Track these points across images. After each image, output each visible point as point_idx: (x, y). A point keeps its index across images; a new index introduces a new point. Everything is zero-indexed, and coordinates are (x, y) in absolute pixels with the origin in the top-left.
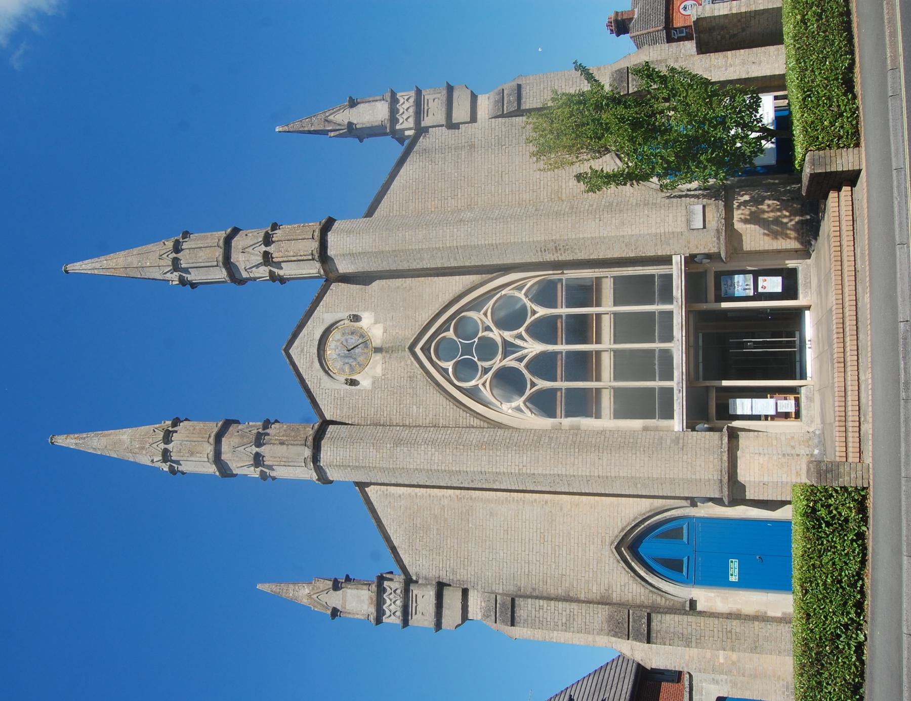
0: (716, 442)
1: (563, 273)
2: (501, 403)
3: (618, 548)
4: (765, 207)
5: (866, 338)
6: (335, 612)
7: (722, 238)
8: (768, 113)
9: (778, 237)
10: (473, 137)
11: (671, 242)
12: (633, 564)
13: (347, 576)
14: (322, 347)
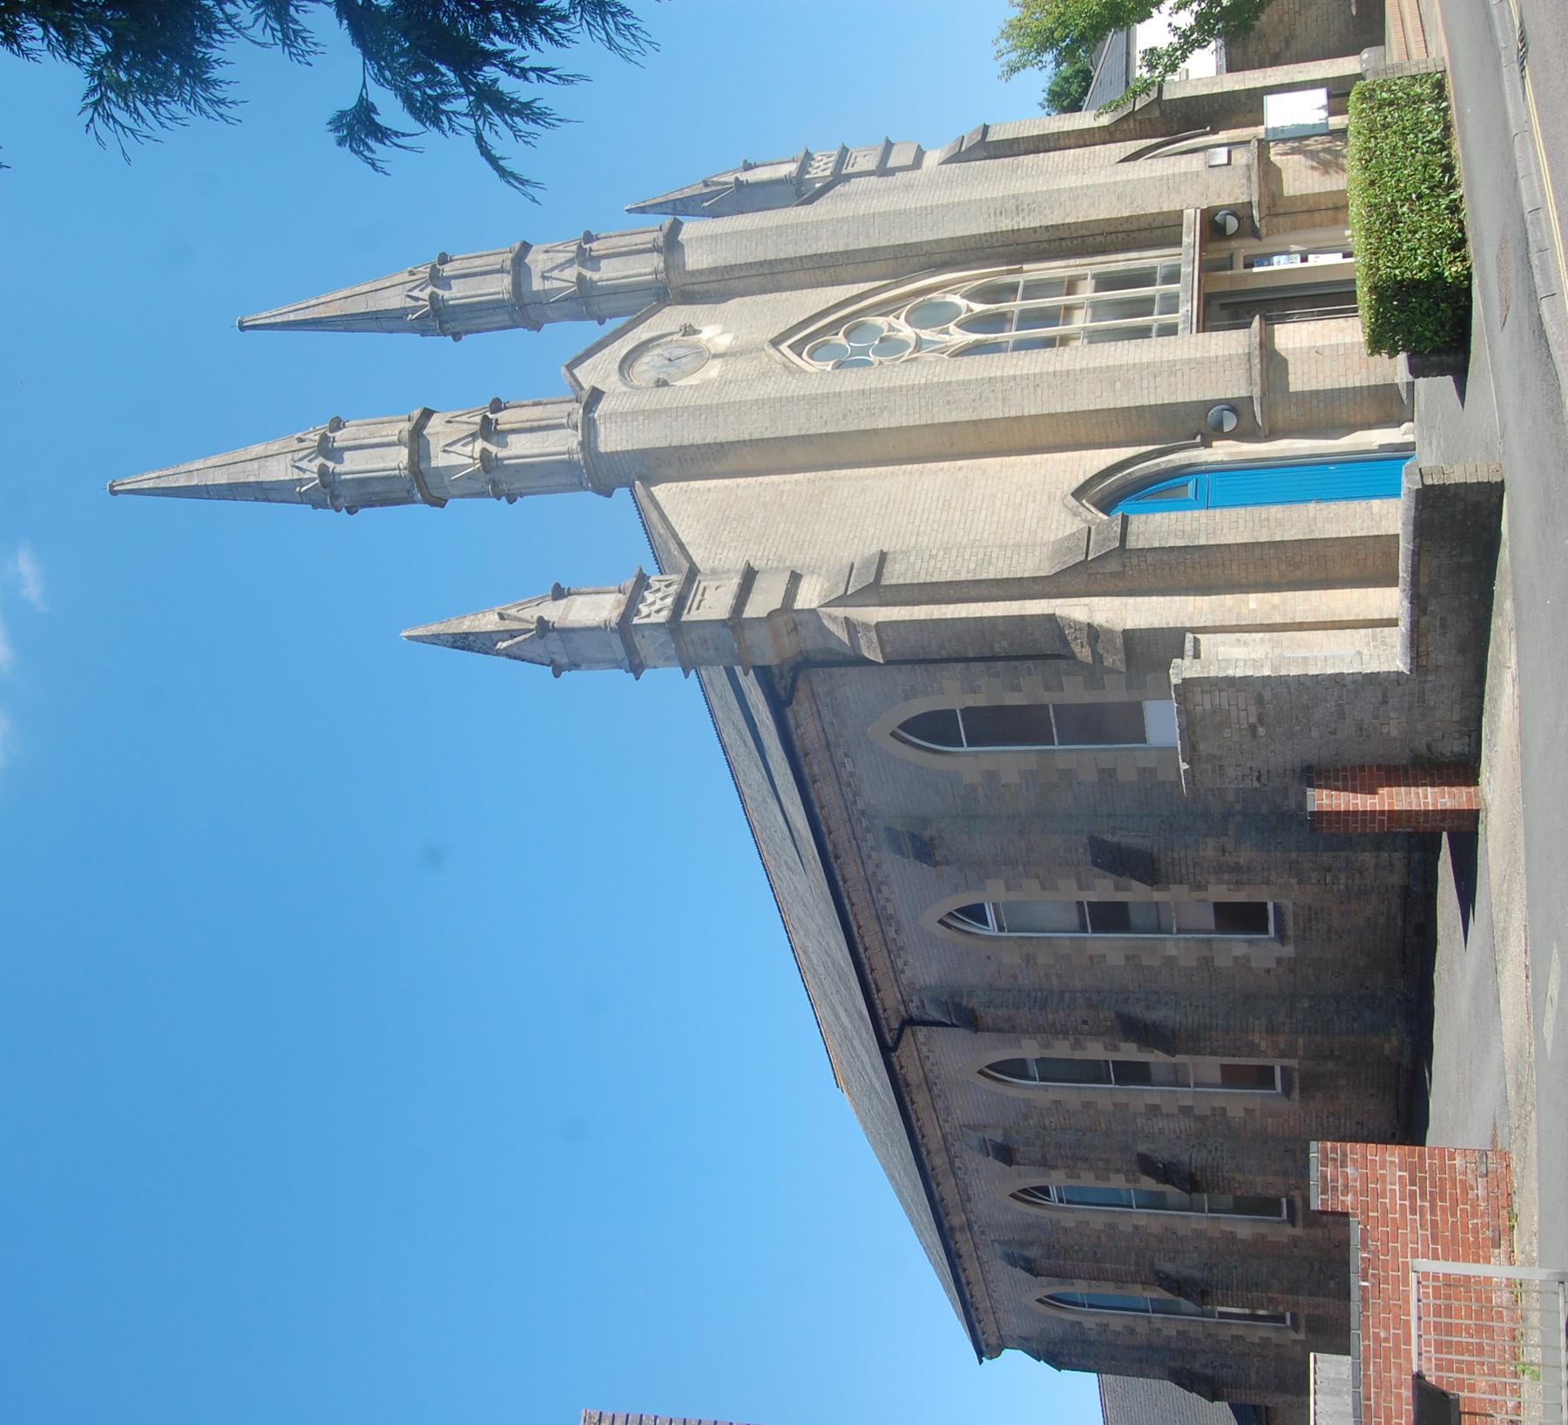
1: (1020, 271)
7: (1255, 178)
9: (1331, 171)
11: (1182, 188)
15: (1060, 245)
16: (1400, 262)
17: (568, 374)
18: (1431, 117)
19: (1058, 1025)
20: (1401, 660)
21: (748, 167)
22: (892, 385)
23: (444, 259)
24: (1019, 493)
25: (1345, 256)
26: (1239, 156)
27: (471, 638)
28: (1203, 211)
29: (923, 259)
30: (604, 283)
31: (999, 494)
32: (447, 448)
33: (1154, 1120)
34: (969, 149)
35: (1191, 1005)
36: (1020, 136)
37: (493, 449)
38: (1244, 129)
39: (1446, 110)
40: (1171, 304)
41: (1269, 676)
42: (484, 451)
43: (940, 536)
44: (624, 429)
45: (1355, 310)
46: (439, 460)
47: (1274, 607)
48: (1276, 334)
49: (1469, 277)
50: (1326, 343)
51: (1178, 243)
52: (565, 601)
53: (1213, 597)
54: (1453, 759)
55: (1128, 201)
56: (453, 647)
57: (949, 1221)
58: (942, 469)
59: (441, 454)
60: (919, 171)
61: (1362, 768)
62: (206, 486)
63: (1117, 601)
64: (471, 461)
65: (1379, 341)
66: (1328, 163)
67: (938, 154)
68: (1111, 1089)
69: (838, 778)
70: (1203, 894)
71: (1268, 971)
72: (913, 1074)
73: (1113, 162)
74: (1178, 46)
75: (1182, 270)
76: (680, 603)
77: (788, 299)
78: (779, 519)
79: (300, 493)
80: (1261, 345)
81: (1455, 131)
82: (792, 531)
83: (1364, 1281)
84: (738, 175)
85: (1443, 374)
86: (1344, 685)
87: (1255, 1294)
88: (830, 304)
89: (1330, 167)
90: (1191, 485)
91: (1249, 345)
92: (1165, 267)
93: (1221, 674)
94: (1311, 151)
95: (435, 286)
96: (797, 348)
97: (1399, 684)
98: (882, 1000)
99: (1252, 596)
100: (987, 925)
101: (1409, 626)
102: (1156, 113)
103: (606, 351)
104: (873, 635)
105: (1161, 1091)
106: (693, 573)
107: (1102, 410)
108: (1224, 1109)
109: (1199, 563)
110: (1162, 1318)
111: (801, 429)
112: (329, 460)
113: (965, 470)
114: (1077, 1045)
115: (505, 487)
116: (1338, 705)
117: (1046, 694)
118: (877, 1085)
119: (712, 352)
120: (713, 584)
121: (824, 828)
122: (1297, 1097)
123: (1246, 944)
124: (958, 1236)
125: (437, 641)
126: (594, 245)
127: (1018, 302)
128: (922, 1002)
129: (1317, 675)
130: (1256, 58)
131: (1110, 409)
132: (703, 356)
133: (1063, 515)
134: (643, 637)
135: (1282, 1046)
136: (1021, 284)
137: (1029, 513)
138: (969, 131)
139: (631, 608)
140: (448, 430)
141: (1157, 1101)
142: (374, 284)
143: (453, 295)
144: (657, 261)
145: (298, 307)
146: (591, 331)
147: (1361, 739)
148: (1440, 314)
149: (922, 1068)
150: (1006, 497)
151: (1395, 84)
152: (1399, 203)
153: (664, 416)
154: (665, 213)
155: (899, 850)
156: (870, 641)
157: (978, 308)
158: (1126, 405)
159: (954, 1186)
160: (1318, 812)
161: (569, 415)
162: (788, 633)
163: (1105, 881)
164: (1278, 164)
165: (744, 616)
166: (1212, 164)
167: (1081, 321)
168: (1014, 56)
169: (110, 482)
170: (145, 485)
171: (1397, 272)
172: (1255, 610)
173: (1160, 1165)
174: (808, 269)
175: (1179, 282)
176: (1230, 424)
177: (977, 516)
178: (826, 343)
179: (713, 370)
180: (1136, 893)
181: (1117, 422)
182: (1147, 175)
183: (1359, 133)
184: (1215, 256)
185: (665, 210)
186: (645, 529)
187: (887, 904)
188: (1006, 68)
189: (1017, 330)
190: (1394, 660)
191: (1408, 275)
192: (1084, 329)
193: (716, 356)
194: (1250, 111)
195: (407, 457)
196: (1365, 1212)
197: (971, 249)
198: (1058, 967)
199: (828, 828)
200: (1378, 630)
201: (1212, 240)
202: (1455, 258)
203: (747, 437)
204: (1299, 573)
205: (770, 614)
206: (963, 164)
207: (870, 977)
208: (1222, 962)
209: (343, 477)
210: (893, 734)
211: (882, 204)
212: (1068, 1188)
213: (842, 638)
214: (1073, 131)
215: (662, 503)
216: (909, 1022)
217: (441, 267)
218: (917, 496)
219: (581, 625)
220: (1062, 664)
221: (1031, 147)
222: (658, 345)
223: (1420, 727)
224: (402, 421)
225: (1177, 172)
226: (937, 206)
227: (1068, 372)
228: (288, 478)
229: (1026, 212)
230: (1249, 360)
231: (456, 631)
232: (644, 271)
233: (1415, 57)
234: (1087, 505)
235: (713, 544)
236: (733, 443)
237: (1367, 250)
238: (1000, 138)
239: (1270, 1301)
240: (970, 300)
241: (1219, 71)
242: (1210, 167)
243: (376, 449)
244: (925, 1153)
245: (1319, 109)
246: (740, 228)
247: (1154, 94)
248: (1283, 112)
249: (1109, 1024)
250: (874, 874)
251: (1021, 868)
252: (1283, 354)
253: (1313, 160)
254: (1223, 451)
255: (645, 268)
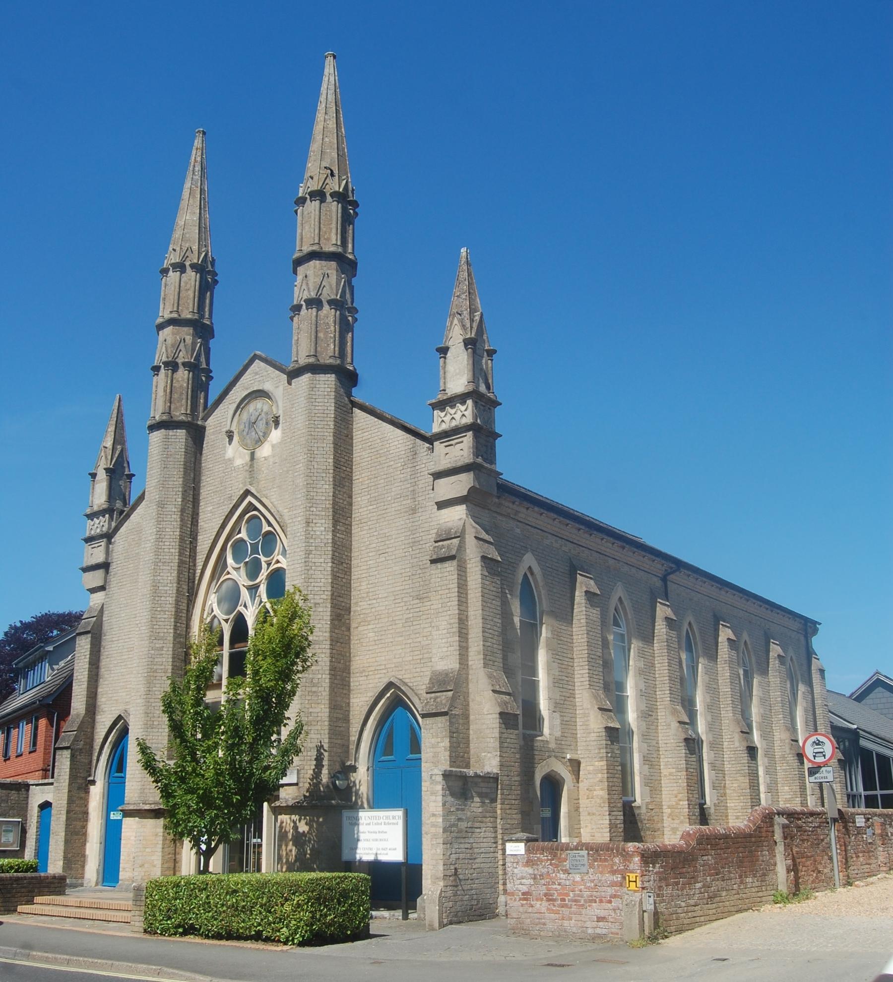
0: (151, 799)
2: (215, 593)
3: (390, 685)
4: (290, 846)
5: (68, 925)
6: (443, 351)
8: (387, 854)
10: (423, 509)
12: (383, 700)
13: (495, 352)
14: (257, 394)
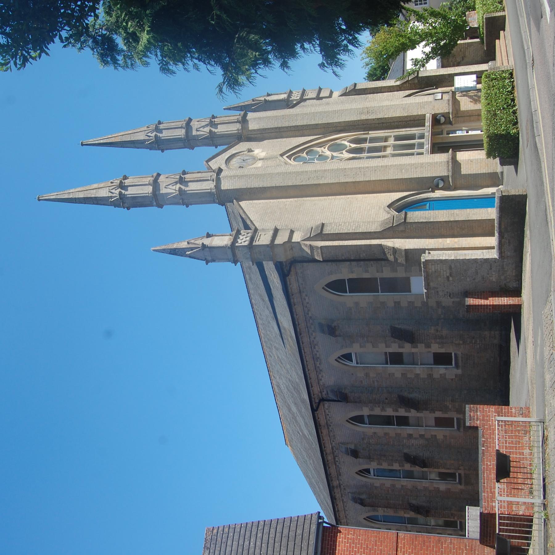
1: (368, 134)
7: (451, 104)
11: (425, 107)
15: (382, 125)
16: (497, 128)
17: (207, 164)
18: (508, 84)
19: (377, 400)
20: (496, 254)
21: (269, 95)
22: (325, 169)
23: (160, 123)
24: (369, 206)
25: (481, 132)
26: (445, 96)
27: (177, 250)
28: (432, 115)
29: (334, 128)
30: (219, 133)
31: (362, 206)
32: (166, 187)
33: (410, 440)
34: (349, 92)
35: (425, 392)
36: (368, 87)
37: (183, 187)
38: (447, 88)
39: (513, 81)
40: (421, 146)
41: (453, 259)
42: (180, 188)
43: (342, 220)
44: (231, 181)
45: (484, 149)
46: (163, 191)
47: (455, 242)
48: (457, 155)
49: (518, 134)
50: (474, 158)
51: (424, 125)
52: (211, 238)
53: (435, 239)
54: (513, 289)
55: (407, 110)
56: (170, 254)
57: (332, 483)
58: (342, 198)
59: (164, 189)
60: (331, 98)
61: (484, 292)
62: (75, 198)
63: (403, 240)
64: (175, 191)
65: (490, 154)
66: (476, 100)
67: (338, 93)
68: (395, 428)
69: (303, 304)
70: (429, 349)
71: (452, 380)
72: (322, 421)
73: (400, 97)
74: (425, 58)
75: (425, 134)
76: (252, 239)
77: (285, 141)
78: (285, 213)
79: (111, 201)
80: (452, 158)
81: (515, 88)
82: (290, 217)
83: (483, 447)
84: (265, 98)
85: (510, 165)
86: (478, 263)
87: (446, 511)
88: (301, 143)
89: (477, 101)
90: (428, 205)
91: (448, 158)
92: (419, 134)
93: (438, 258)
94: (470, 96)
95: (157, 132)
96: (289, 157)
97: (495, 262)
98: (313, 391)
99: (448, 239)
100: (352, 362)
101: (498, 242)
102: (416, 81)
103: (220, 157)
104: (319, 251)
105: (413, 428)
106: (256, 230)
107: (398, 179)
108: (436, 436)
109: (431, 228)
110: (411, 526)
111: (293, 183)
112: (123, 190)
113: (350, 198)
114: (383, 409)
115: (186, 201)
116: (476, 270)
117: (377, 274)
118: (306, 432)
119: (259, 158)
120: (264, 233)
121: (297, 323)
122: (462, 430)
123: (445, 369)
124: (336, 490)
125: (165, 252)
126: (216, 120)
127: (367, 144)
128: (327, 392)
129: (469, 259)
130: (452, 63)
131: (400, 179)
132: (255, 159)
133: (384, 213)
134: (239, 250)
135: (457, 407)
136: (368, 138)
137: (373, 212)
138: (349, 85)
139: (235, 241)
140: (167, 180)
141: (411, 433)
142: (133, 131)
143: (163, 136)
144: (238, 126)
145: (104, 138)
146: (212, 150)
147: (483, 282)
148: (509, 145)
149: (326, 419)
150: (364, 207)
151: (497, 73)
152: (497, 110)
153: (245, 177)
154: (238, 110)
155: (323, 331)
156: (318, 253)
157: (353, 146)
158: (406, 177)
159: (335, 468)
160: (469, 305)
161: (211, 176)
162: (289, 250)
163: (395, 344)
164: (459, 100)
165: (275, 243)
166: (436, 99)
167: (389, 151)
168: (367, 60)
169: (38, 196)
170: (52, 197)
171: (496, 131)
172: (449, 243)
173: (412, 457)
174: (293, 131)
175: (424, 139)
176: (441, 185)
177: (354, 213)
178: (299, 156)
179: (259, 164)
180: (407, 349)
181: (403, 183)
182: (413, 102)
183: (485, 88)
184: (437, 130)
185: (237, 109)
186: (229, 222)
187: (317, 353)
188: (365, 64)
189: (367, 153)
190: (494, 255)
191: (499, 132)
192: (391, 153)
193: (260, 159)
194: (449, 82)
195: (152, 189)
196: (484, 426)
197: (351, 126)
198: (377, 378)
199: (298, 322)
200: (490, 250)
201: (435, 125)
202: (514, 128)
203: (274, 186)
204: (464, 232)
205: (284, 243)
206: (347, 97)
207: (309, 381)
208: (436, 376)
209: (128, 196)
210: (323, 288)
211: (320, 109)
212: (378, 469)
213: (308, 252)
214: (387, 86)
215: (243, 207)
216: (322, 400)
217: (159, 126)
218: (333, 206)
219: (217, 246)
220: (383, 262)
221: (372, 92)
222: (239, 155)
223: (502, 277)
224: (149, 177)
225: (424, 101)
226: (339, 110)
227: (386, 166)
228: (106, 196)
229: (371, 113)
230: (448, 163)
231: (172, 248)
232: (234, 129)
233: (504, 65)
234: (392, 210)
235: (262, 221)
236: (269, 187)
237: (486, 125)
238: (361, 88)
239: (452, 514)
240: (351, 143)
241: (438, 67)
242: (435, 100)
243: (140, 187)
244: (325, 454)
245: (473, 81)
246: (269, 115)
247: (416, 75)
248: (462, 82)
249: (395, 399)
250: (313, 341)
251: (366, 339)
252: (460, 162)
253: (471, 99)
254: (438, 194)
255: (234, 128)
